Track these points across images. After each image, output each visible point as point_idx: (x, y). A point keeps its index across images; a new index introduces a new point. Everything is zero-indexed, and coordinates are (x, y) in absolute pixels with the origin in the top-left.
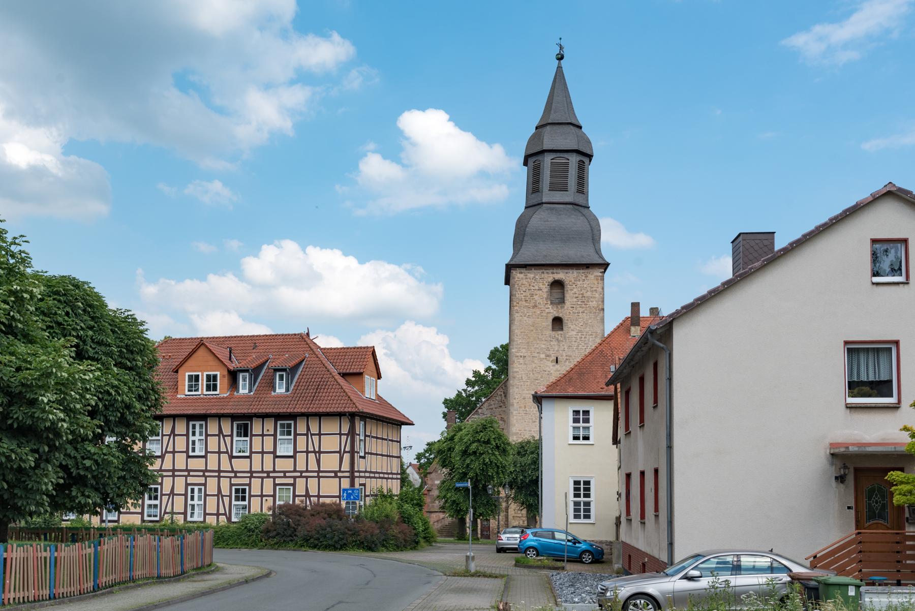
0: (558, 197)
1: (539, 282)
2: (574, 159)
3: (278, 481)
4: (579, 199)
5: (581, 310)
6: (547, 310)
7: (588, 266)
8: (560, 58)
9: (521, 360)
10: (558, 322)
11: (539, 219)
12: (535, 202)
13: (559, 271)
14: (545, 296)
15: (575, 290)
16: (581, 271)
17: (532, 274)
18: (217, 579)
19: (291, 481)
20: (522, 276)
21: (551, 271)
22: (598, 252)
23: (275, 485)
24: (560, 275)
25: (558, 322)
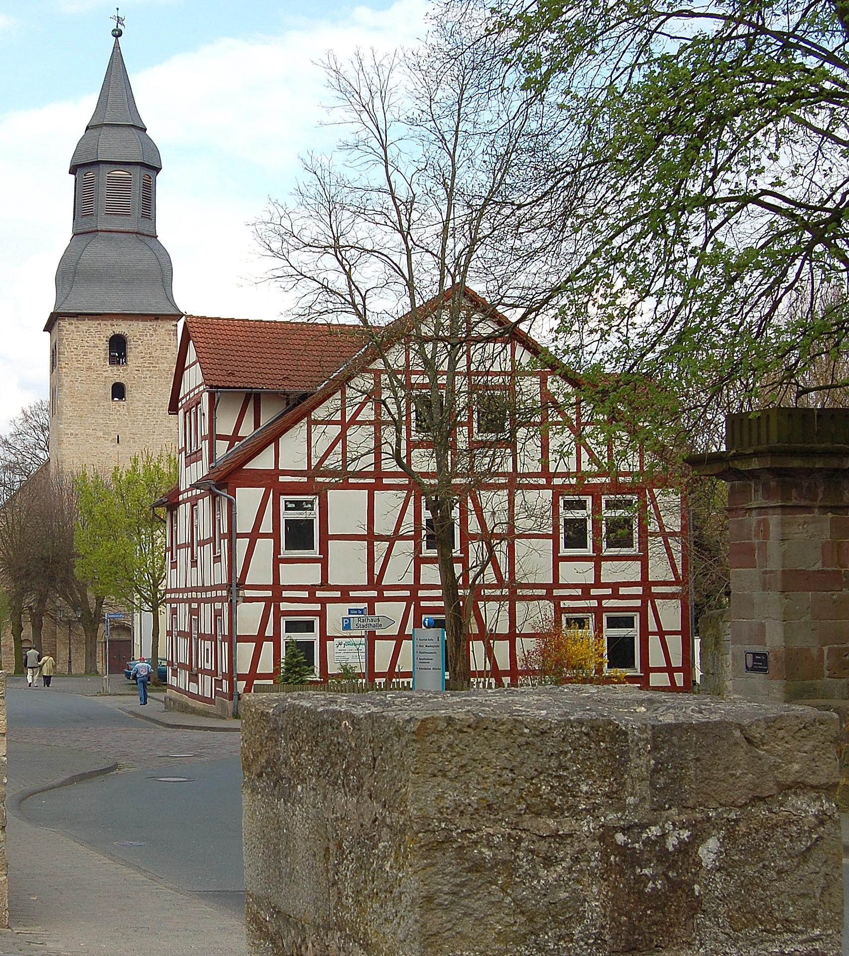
0: (117, 223)
1: (92, 338)
2: (138, 172)
3: (564, 604)
4: (144, 227)
5: (149, 374)
6: (105, 374)
7: (156, 317)
8: (117, 34)
9: (73, 440)
10: (118, 391)
11: (100, 252)
12: (87, 228)
13: (120, 322)
14: (103, 355)
15: (141, 348)
16: (149, 323)
17: (85, 325)
18: (819, 707)
19: (317, 607)
20: (72, 327)
21: (109, 323)
22: (170, 298)
23: (558, 611)
24: (122, 328)
25: (118, 391)
